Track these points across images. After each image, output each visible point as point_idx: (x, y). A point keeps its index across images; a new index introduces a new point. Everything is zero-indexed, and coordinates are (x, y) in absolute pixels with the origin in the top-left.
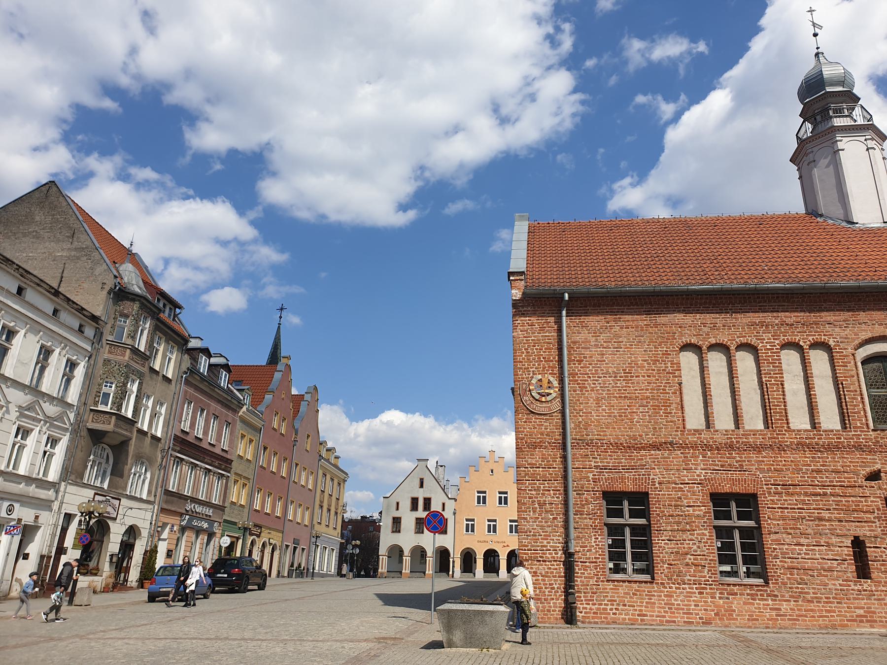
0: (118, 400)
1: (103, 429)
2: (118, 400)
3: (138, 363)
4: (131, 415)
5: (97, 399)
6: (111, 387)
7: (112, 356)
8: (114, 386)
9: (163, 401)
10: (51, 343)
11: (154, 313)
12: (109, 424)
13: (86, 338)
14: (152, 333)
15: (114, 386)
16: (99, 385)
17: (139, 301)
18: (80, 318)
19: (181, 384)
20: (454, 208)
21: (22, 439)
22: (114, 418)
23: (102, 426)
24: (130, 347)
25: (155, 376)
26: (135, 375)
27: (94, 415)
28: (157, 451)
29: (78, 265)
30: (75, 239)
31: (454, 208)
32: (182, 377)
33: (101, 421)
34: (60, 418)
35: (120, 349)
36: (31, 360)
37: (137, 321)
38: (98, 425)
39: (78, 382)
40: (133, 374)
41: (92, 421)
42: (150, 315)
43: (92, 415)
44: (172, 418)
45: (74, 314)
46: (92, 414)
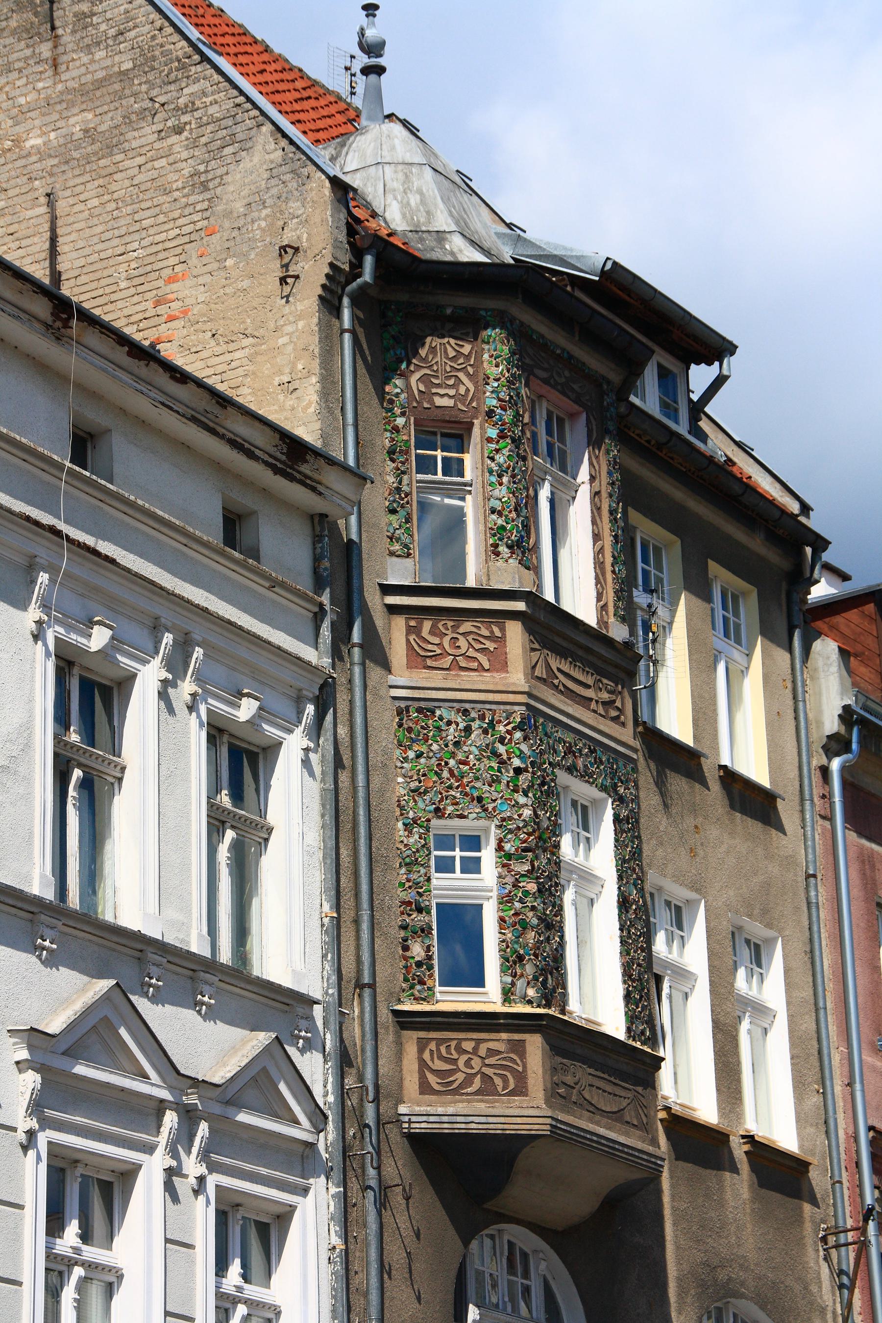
0: (531, 937)
1: (496, 1126)
2: (531, 937)
3: (585, 702)
4: (623, 1029)
5: (417, 950)
6: (472, 866)
7: (436, 679)
8: (488, 856)
9: (757, 929)
10: (107, 634)
11: (597, 381)
12: (521, 1090)
13: (274, 584)
14: (612, 512)
15: (488, 856)
16: (410, 864)
17: (502, 320)
18: (218, 467)
19: (829, 818)
20: (809, 550)
21: (86, 1236)
22: (535, 1044)
23: (481, 1107)
24: (521, 606)
25: (677, 783)
26: (586, 776)
27: (422, 1045)
28: (800, 1243)
29: (120, 186)
30: (67, 37)
31: (809, 550)
32: (825, 771)
33: (469, 1080)
34: (254, 1079)
35: (467, 627)
36: (27, 746)
37: (517, 442)
38: (461, 1107)
39: (297, 859)
40: (571, 770)
41: (425, 1088)
42: (578, 401)
43: (411, 1049)
44: (832, 1029)
45: (185, 447)
46: (411, 1038)
